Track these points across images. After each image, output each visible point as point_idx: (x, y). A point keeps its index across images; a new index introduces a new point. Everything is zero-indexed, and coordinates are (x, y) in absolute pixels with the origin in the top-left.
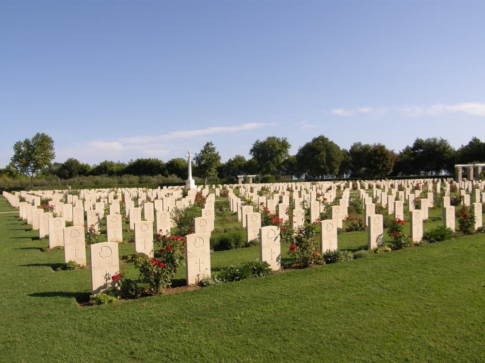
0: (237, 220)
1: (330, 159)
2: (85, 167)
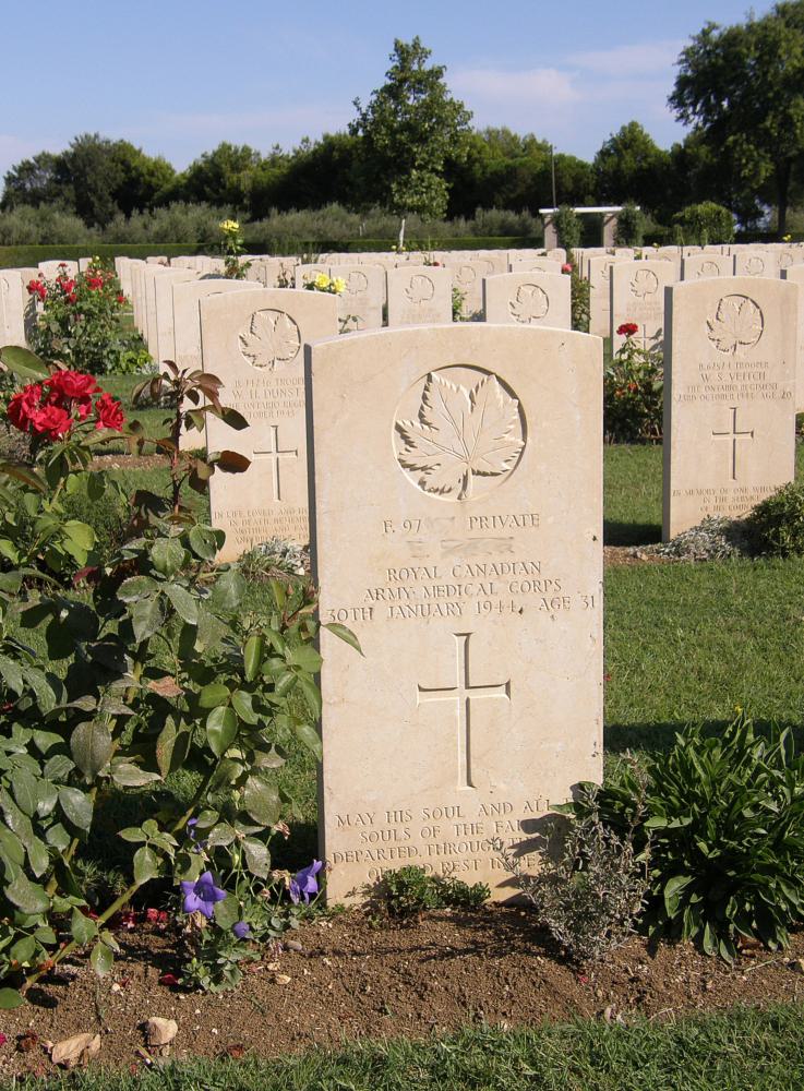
2: (152, 174)
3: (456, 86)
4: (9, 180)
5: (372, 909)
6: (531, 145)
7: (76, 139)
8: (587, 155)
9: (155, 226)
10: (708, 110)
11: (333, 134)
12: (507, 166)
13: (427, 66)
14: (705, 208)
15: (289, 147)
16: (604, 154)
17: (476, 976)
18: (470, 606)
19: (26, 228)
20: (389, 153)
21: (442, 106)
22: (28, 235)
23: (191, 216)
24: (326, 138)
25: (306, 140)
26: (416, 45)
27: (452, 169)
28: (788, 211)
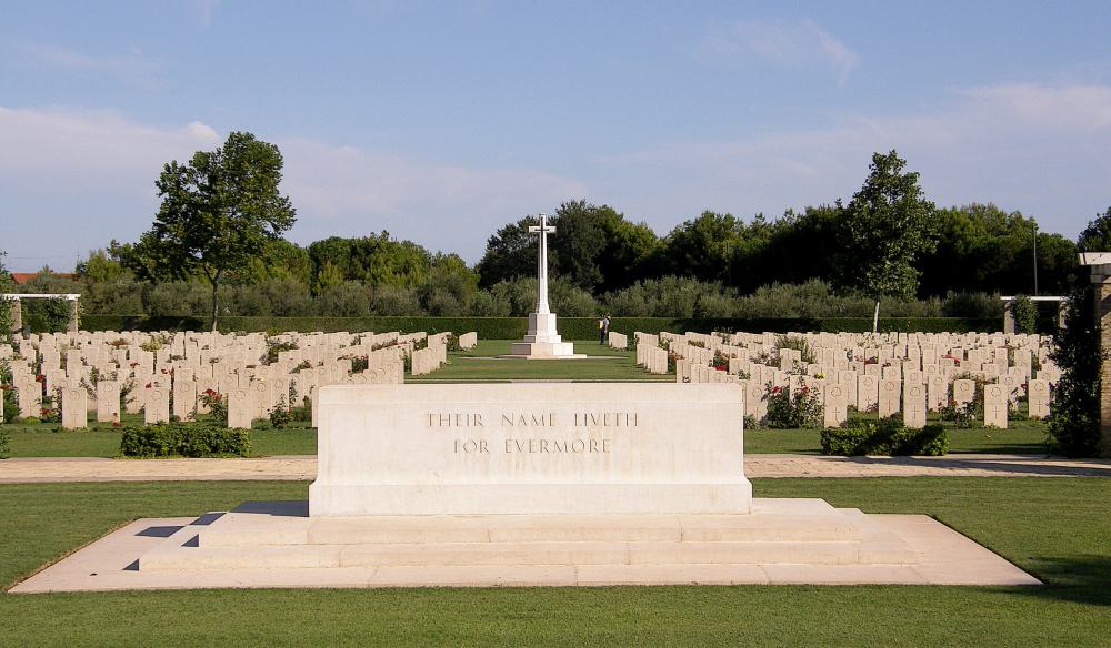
2: (633, 240)
6: (1017, 222)
7: (563, 206)
11: (816, 207)
12: (990, 244)
13: (903, 172)
15: (773, 216)
23: (688, 290)
24: (809, 210)
25: (789, 212)
26: (893, 155)
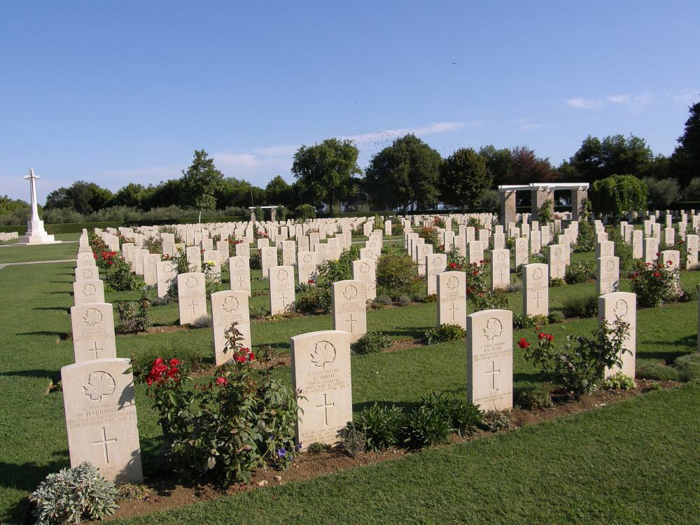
0: (407, 255)
1: (415, 177)
2: (104, 195)
3: (217, 166)
4: (49, 198)
5: (309, 452)
6: (243, 183)
8: (263, 187)
9: (107, 215)
10: (304, 173)
13: (207, 159)
14: (306, 206)
15: (156, 184)
16: (269, 186)
17: (334, 462)
18: (326, 388)
19: (59, 217)
20: (195, 189)
21: (213, 172)
22: (60, 220)
23: (122, 211)
24: (169, 181)
26: (203, 152)
27: (218, 194)
28: (333, 206)
